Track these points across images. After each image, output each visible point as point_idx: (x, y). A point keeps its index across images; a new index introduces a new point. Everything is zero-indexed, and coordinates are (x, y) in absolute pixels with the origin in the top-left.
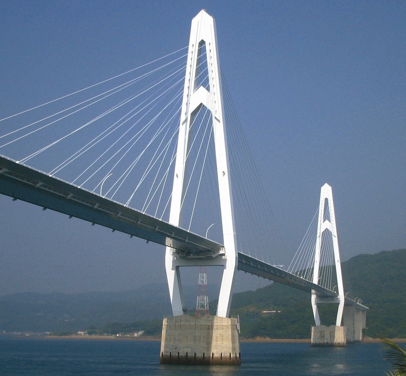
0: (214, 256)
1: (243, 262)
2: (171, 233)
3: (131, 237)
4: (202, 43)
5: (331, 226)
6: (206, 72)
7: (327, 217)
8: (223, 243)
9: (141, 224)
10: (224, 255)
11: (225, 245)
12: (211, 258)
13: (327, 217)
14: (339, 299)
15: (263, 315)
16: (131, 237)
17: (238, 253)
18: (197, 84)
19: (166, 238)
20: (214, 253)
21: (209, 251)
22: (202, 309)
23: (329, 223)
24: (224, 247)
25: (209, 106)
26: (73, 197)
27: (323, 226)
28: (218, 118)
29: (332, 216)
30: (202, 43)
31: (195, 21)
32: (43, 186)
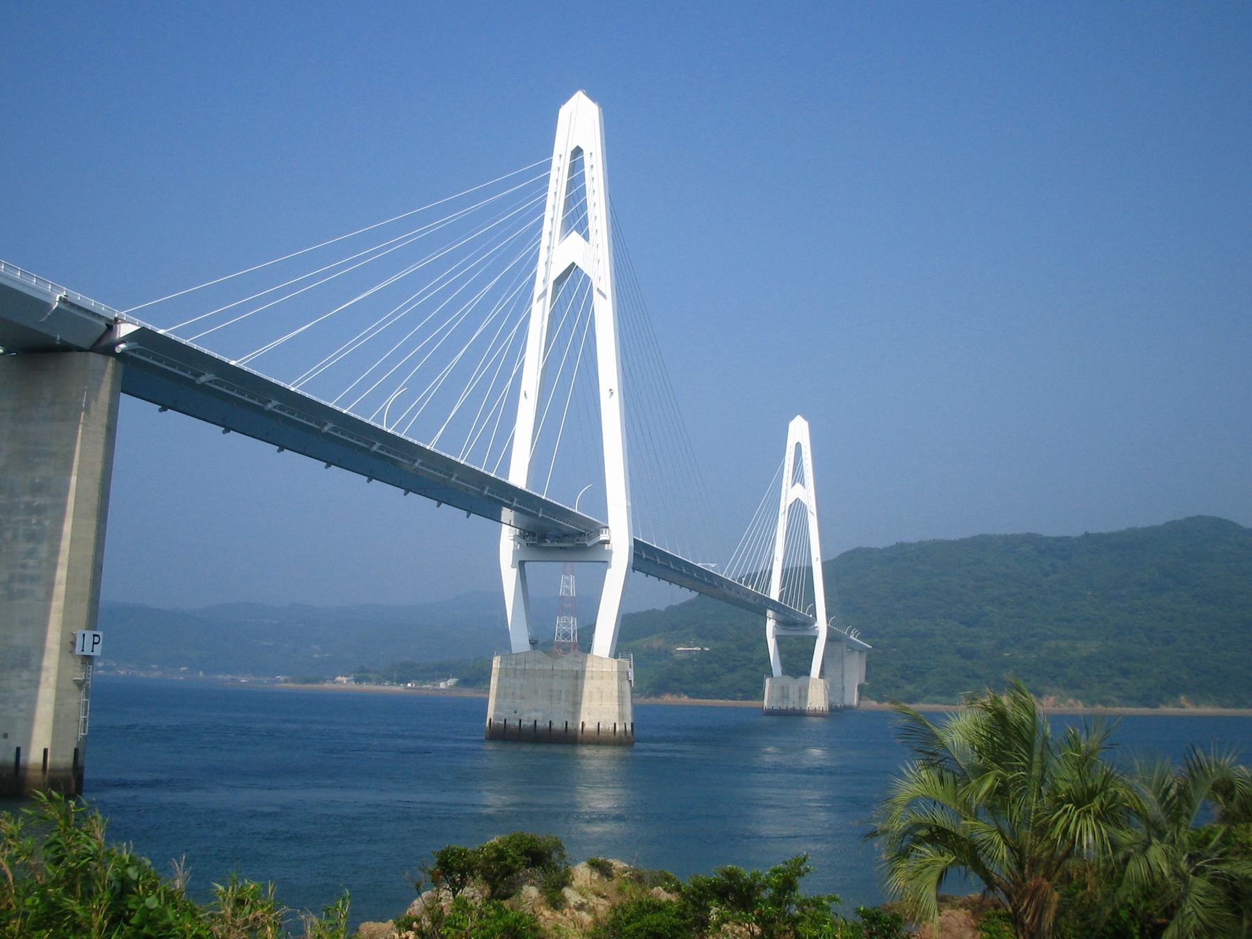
0: (589, 544)
2: (512, 500)
4: (577, 152)
5: (806, 494)
7: (575, 220)
8: (606, 520)
10: (607, 542)
11: (610, 524)
17: (636, 541)
19: (502, 509)
21: (581, 534)
22: (566, 640)
23: (803, 488)
24: (608, 527)
27: (791, 493)
30: (577, 152)
31: (565, 112)
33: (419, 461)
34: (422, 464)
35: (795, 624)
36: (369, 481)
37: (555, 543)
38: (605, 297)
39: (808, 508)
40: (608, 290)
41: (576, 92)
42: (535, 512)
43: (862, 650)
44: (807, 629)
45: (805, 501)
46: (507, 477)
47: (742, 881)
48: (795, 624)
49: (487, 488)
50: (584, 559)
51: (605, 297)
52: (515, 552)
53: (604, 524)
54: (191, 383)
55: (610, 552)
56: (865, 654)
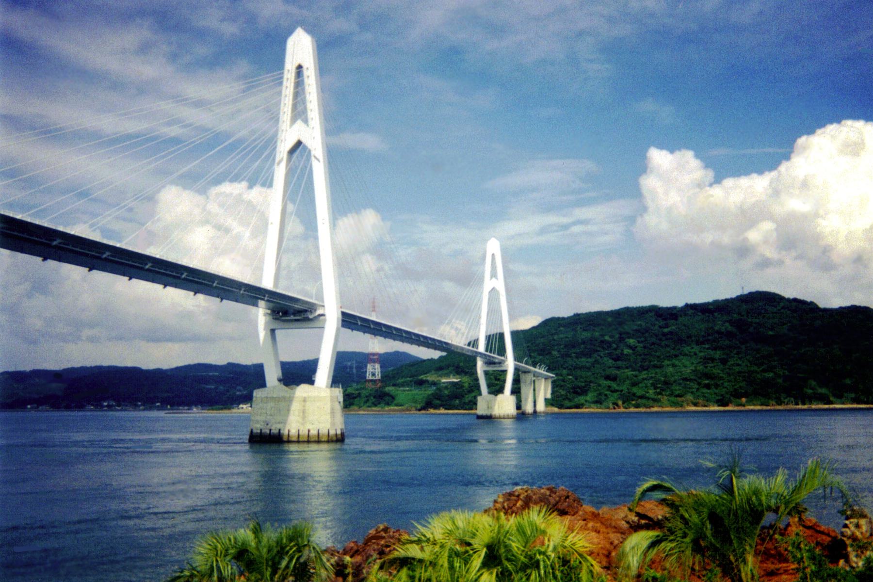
0: (311, 317)
1: (357, 324)
2: (264, 296)
3: (221, 301)
4: (300, 67)
5: (499, 284)
6: (304, 102)
7: (494, 275)
8: (323, 301)
9: (218, 285)
10: (323, 315)
11: (326, 304)
12: (307, 320)
13: (494, 275)
14: (322, 318)
15: (442, 385)
16: (221, 301)
17: (343, 314)
18: (294, 120)
19: (258, 302)
20: (311, 312)
21: (306, 311)
22: (374, 378)
23: (306, 126)
24: (323, 306)
25: (498, 288)
26: (151, 266)
27: (489, 284)
28: (318, 157)
29: (311, 108)
30: (300, 67)
31: (291, 42)
32: (111, 256)
33: (216, 282)
34: (245, 291)
35: (494, 363)
36: (90, 271)
37: (292, 316)
38: (318, 160)
39: (313, 153)
40: (321, 158)
41: (297, 27)
42: (210, 283)
43: (546, 378)
44: (501, 366)
45: (498, 289)
46: (261, 282)
47: (835, 346)
48: (494, 363)
49: (267, 295)
50: (306, 326)
51: (318, 160)
52: (266, 323)
53: (321, 303)
54: (142, 269)
55: (325, 320)
56: (550, 381)
